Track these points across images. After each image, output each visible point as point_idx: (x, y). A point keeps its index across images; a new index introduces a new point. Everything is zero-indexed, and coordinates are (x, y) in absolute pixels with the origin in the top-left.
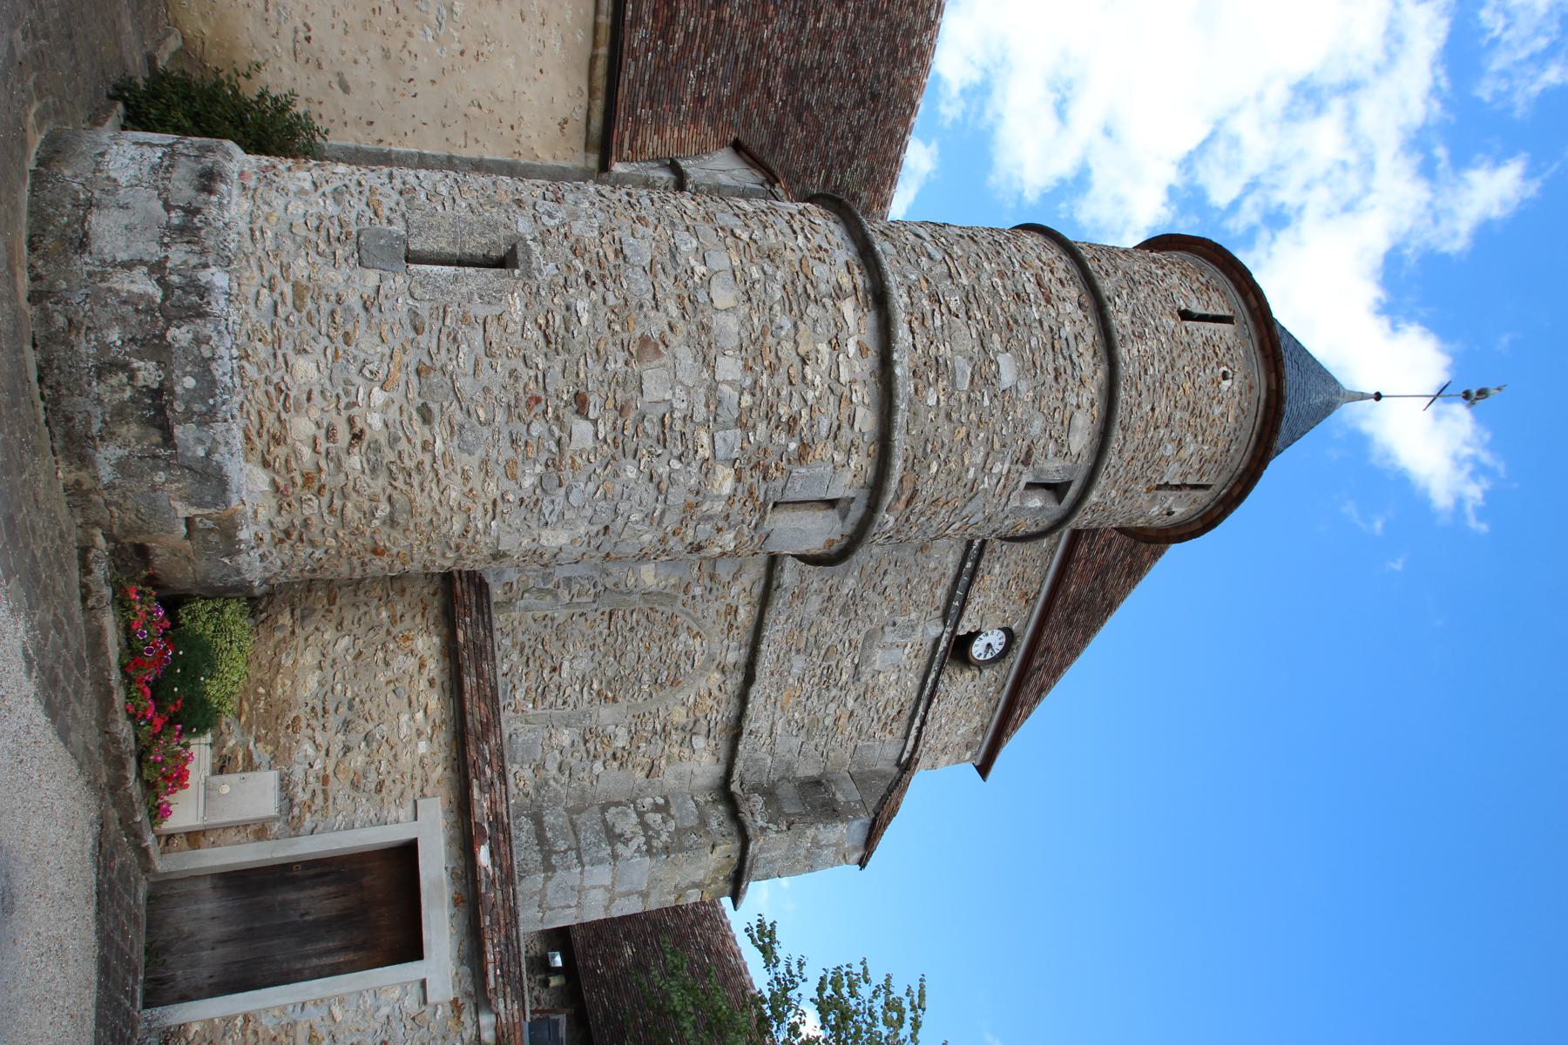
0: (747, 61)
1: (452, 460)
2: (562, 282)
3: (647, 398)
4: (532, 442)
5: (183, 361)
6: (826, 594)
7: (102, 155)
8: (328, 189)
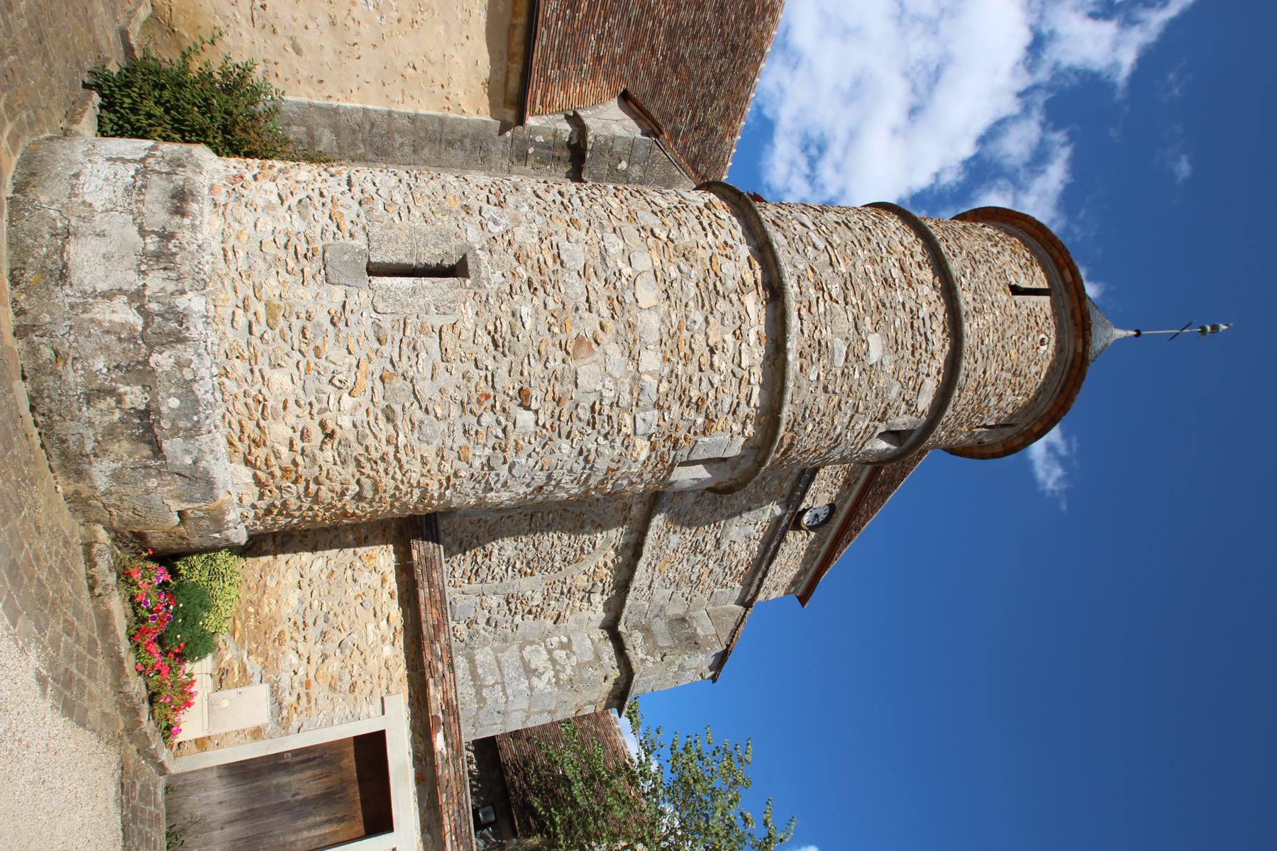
0: (638, 23)
2: (508, 290)
3: (580, 390)
5: (167, 384)
7: (77, 176)
8: (293, 201)
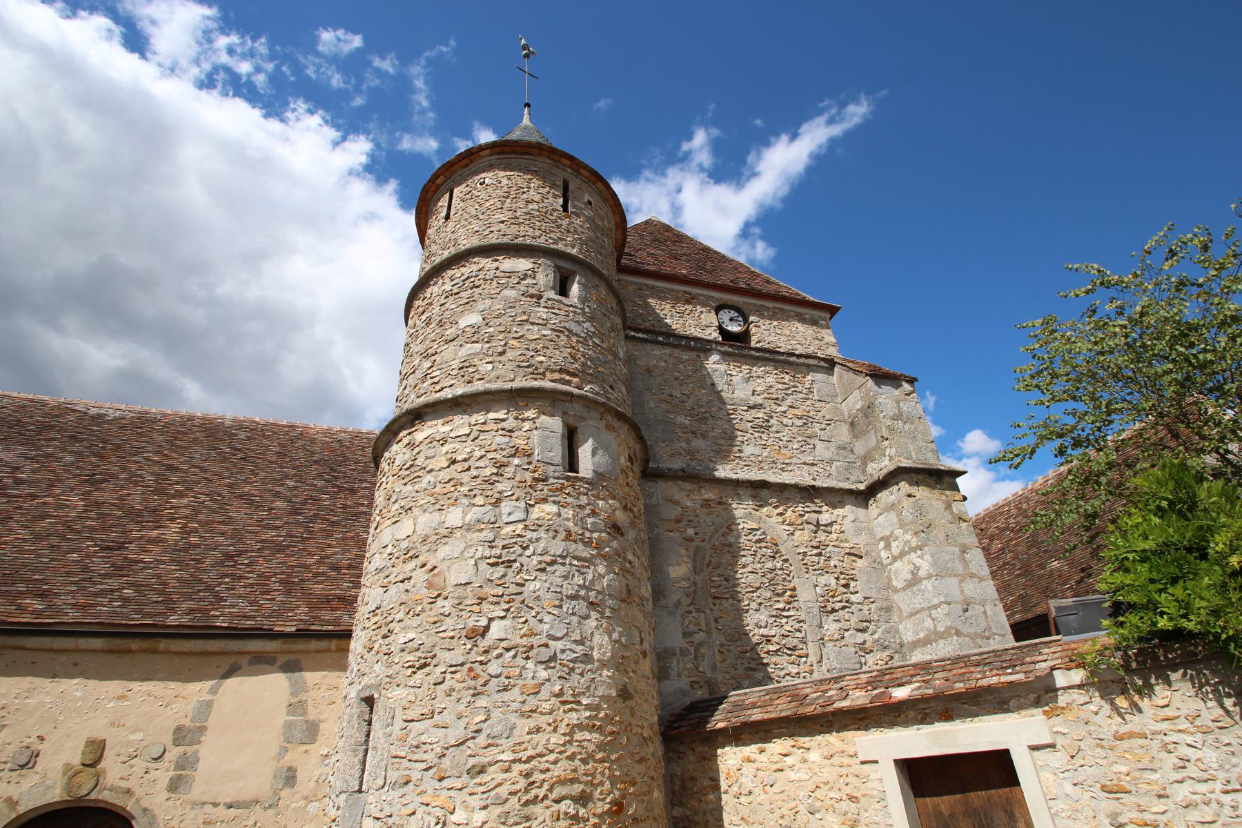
1: (519, 744)
2: (386, 657)
4: (506, 671)
6: (690, 435)
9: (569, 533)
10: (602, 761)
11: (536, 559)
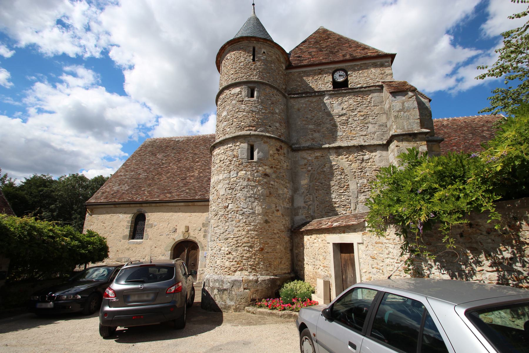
6: (313, 132)
9: (249, 179)
10: (257, 238)
11: (239, 187)
